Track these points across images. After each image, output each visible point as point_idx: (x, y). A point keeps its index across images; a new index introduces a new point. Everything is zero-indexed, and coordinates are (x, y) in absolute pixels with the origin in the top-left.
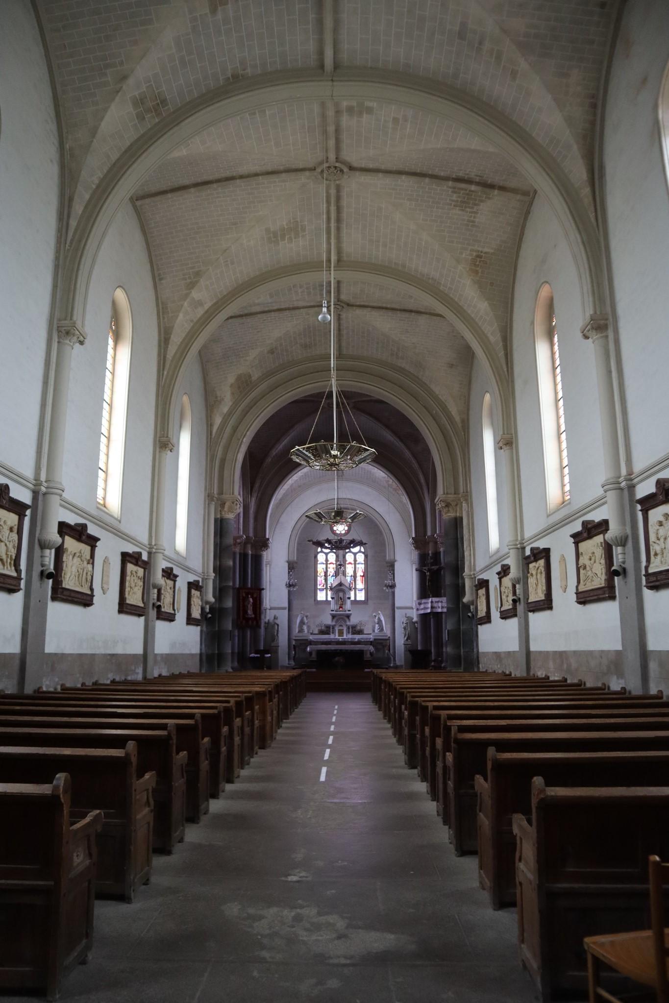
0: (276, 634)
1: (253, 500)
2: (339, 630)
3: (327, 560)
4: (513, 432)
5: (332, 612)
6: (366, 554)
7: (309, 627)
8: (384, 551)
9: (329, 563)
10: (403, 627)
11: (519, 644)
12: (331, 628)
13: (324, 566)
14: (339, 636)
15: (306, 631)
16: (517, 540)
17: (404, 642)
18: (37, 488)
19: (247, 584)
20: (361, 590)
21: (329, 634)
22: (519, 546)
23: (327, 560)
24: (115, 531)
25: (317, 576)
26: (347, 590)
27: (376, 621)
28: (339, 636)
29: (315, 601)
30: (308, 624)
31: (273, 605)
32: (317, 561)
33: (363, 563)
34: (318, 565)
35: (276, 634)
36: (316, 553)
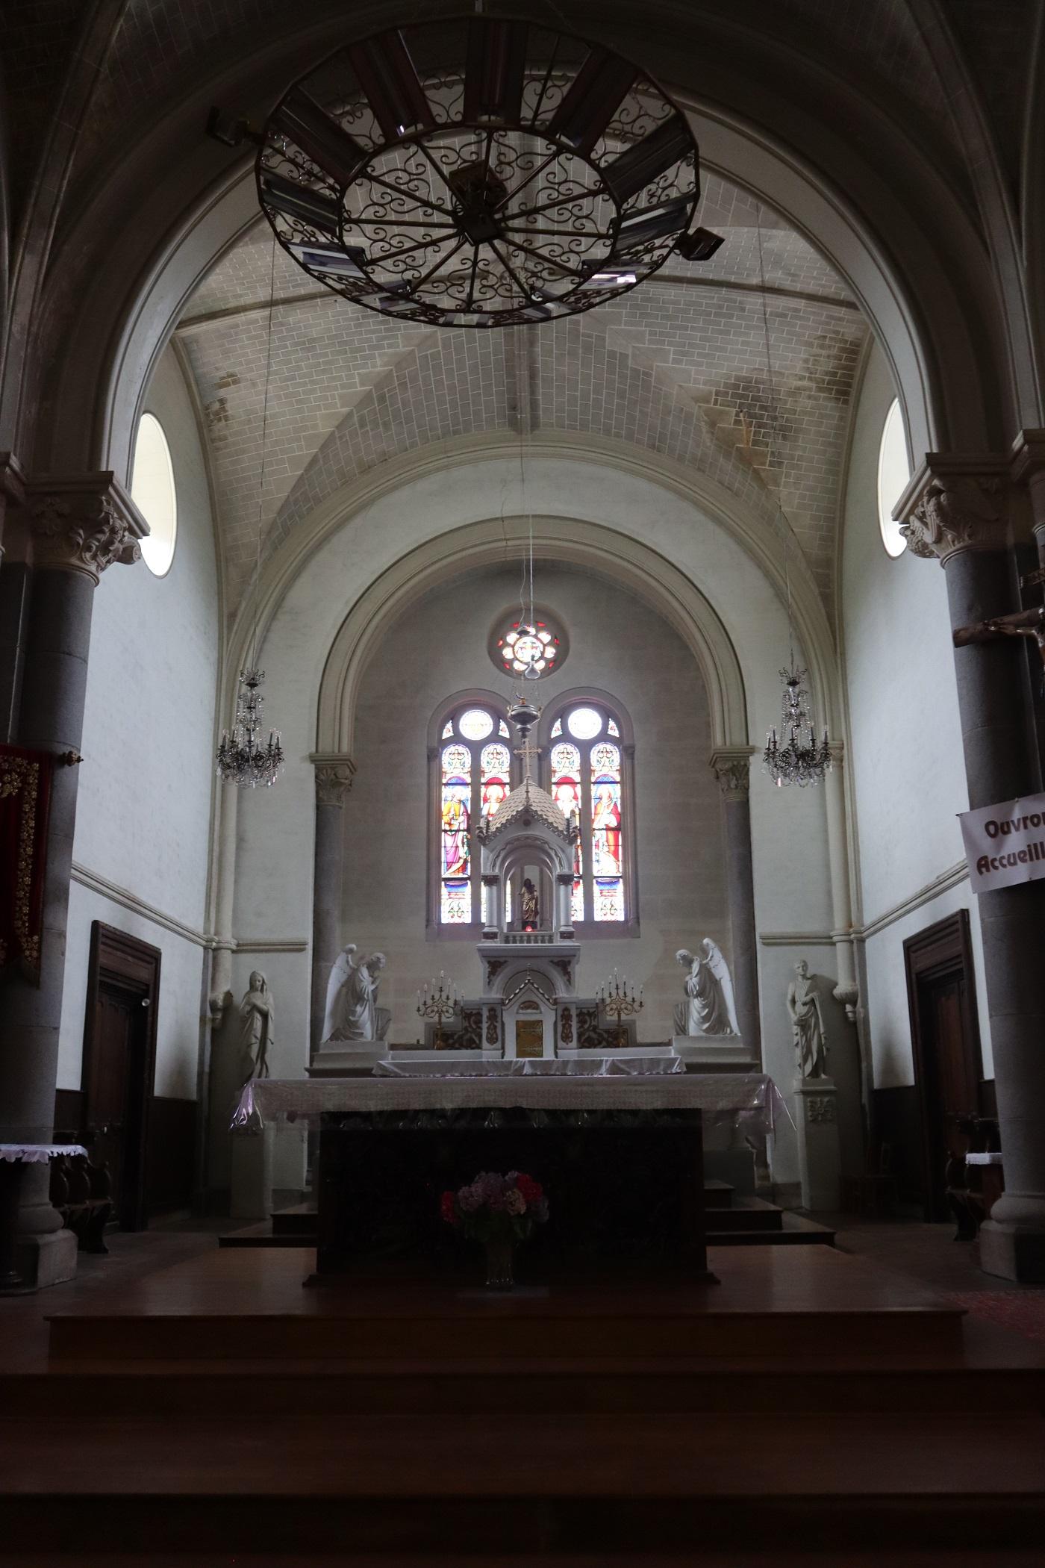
1: (30, 267)
3: (476, 771)
4: (845, 739)
6: (627, 742)
7: (382, 1017)
9: (483, 780)
10: (794, 1018)
12: (485, 1013)
13: (466, 793)
14: (520, 1053)
15: (368, 1031)
16: (850, 926)
17: (804, 1082)
18: (208, 943)
20: (612, 881)
21: (473, 1044)
22: (853, 936)
23: (476, 771)
24: (188, 934)
25: (440, 831)
27: (693, 981)
29: (428, 921)
30: (381, 1002)
31: (252, 935)
33: (618, 779)
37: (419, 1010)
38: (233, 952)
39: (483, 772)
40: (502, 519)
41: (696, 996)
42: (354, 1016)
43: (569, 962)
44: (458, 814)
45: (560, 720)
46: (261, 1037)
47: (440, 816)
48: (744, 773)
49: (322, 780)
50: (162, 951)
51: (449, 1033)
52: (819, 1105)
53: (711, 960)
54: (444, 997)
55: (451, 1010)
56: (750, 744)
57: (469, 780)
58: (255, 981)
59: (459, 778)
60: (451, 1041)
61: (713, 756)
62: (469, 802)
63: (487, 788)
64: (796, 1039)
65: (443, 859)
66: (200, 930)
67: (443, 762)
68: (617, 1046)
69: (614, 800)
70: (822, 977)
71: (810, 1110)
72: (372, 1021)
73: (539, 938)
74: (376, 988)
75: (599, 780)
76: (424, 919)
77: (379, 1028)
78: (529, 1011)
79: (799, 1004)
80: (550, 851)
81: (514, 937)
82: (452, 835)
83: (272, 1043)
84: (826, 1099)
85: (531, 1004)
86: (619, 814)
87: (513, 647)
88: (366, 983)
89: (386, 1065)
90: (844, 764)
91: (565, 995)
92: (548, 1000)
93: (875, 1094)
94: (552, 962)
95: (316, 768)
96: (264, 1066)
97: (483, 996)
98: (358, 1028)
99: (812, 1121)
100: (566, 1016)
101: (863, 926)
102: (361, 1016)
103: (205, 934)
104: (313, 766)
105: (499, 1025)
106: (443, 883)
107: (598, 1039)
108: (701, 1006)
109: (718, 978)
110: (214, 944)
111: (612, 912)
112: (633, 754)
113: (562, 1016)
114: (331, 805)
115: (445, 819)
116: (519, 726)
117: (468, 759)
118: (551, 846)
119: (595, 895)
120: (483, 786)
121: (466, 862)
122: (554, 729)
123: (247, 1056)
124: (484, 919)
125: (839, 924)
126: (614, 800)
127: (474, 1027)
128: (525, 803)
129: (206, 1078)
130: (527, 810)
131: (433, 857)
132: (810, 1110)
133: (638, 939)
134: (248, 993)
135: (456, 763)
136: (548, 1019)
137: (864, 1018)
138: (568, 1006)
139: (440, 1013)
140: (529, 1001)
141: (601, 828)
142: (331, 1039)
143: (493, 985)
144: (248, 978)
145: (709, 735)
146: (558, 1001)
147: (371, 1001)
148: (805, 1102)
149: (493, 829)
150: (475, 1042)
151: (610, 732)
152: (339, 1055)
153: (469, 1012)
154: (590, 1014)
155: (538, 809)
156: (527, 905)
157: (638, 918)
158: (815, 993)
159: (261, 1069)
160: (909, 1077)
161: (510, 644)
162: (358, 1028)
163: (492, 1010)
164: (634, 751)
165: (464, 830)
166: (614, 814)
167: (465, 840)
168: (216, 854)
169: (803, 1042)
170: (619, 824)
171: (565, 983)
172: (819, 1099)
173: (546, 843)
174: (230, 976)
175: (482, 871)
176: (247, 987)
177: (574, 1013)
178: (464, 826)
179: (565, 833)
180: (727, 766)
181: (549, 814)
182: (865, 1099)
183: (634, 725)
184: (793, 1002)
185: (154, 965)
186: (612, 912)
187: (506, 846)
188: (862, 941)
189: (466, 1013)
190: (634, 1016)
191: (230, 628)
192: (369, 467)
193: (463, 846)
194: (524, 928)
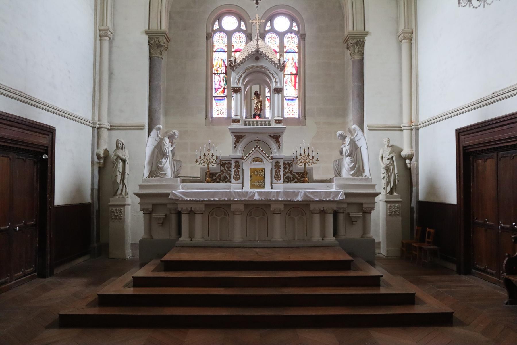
0: (119, 180)
2: (253, 172)
3: (230, 45)
5: (235, 125)
6: (301, 32)
7: (177, 164)
8: (342, 18)
10: (383, 166)
12: (233, 164)
13: (225, 56)
14: (252, 186)
16: (411, 122)
18: (94, 125)
19: (474, 269)
20: (293, 99)
21: (226, 180)
23: (230, 45)
26: (273, 69)
27: (346, 148)
28: (252, 186)
29: (206, 116)
31: (119, 121)
32: (213, 46)
35: (119, 180)
36: (210, 31)
37: (197, 161)
38: (108, 129)
41: (347, 156)
42: (161, 164)
43: (280, 136)
44: (221, 65)
45: (270, 22)
48: (362, 45)
49: (152, 44)
50: (56, 128)
51: (214, 173)
52: (393, 208)
53: (356, 137)
55: (214, 162)
56: (366, 30)
57: (226, 50)
58: (119, 144)
59: (221, 48)
63: (235, 54)
64: (382, 176)
65: (214, 87)
66: (89, 117)
67: (214, 41)
68: (304, 182)
69: (295, 61)
70: (396, 146)
71: (389, 210)
72: (171, 168)
73: (263, 123)
74: (174, 149)
75: (288, 51)
76: (205, 115)
77: (175, 171)
78: (257, 163)
79: (385, 159)
80: (270, 74)
81: (249, 122)
82: (218, 76)
83: (128, 175)
84: (397, 205)
85: (258, 159)
86: (297, 67)
88: (168, 147)
89: (176, 193)
90: (412, 41)
91: (277, 154)
92: (268, 157)
93: (421, 204)
94: (270, 136)
95: (148, 37)
96: (124, 186)
97: (231, 154)
98: (163, 171)
99: (389, 215)
100: (277, 166)
101: (419, 122)
102: (164, 165)
103: (92, 120)
104: (147, 36)
105: (240, 170)
106: (214, 98)
107: (293, 177)
108: (350, 161)
109: (359, 146)
110: (97, 126)
111: (293, 113)
112: (304, 38)
113: (275, 166)
114: (156, 57)
115: (215, 68)
117: (226, 40)
118: (270, 72)
119: (285, 105)
121: (224, 88)
122: (267, 26)
123: (115, 181)
125: (405, 121)
126: (295, 61)
127: (227, 170)
128: (256, 47)
129: (96, 192)
130: (257, 51)
132: (389, 210)
133: (305, 126)
134: (115, 150)
135: (220, 41)
136: (268, 167)
138: (279, 160)
139: (208, 163)
140: (258, 158)
141: (288, 74)
142: (149, 177)
143: (238, 148)
144: (116, 143)
145: (342, 27)
146: (274, 157)
148: (386, 206)
149: (238, 62)
150: (227, 178)
151: (294, 28)
152: (154, 185)
153: (224, 162)
154: (289, 164)
156: (256, 105)
157: (305, 116)
158: (393, 154)
160: (452, 198)
163: (237, 162)
165: (224, 74)
166: (294, 67)
167: (224, 78)
170: (297, 72)
171: (277, 148)
174: (107, 142)
175: (232, 85)
176: (115, 147)
177: (281, 164)
178: (224, 71)
180: (354, 41)
181: (269, 55)
182: (414, 204)
183: (306, 25)
184: (382, 158)
185: (50, 136)
186: (293, 113)
187: (245, 71)
188: (418, 129)
189: (222, 163)
190: (313, 166)
193: (223, 81)
194: (254, 117)
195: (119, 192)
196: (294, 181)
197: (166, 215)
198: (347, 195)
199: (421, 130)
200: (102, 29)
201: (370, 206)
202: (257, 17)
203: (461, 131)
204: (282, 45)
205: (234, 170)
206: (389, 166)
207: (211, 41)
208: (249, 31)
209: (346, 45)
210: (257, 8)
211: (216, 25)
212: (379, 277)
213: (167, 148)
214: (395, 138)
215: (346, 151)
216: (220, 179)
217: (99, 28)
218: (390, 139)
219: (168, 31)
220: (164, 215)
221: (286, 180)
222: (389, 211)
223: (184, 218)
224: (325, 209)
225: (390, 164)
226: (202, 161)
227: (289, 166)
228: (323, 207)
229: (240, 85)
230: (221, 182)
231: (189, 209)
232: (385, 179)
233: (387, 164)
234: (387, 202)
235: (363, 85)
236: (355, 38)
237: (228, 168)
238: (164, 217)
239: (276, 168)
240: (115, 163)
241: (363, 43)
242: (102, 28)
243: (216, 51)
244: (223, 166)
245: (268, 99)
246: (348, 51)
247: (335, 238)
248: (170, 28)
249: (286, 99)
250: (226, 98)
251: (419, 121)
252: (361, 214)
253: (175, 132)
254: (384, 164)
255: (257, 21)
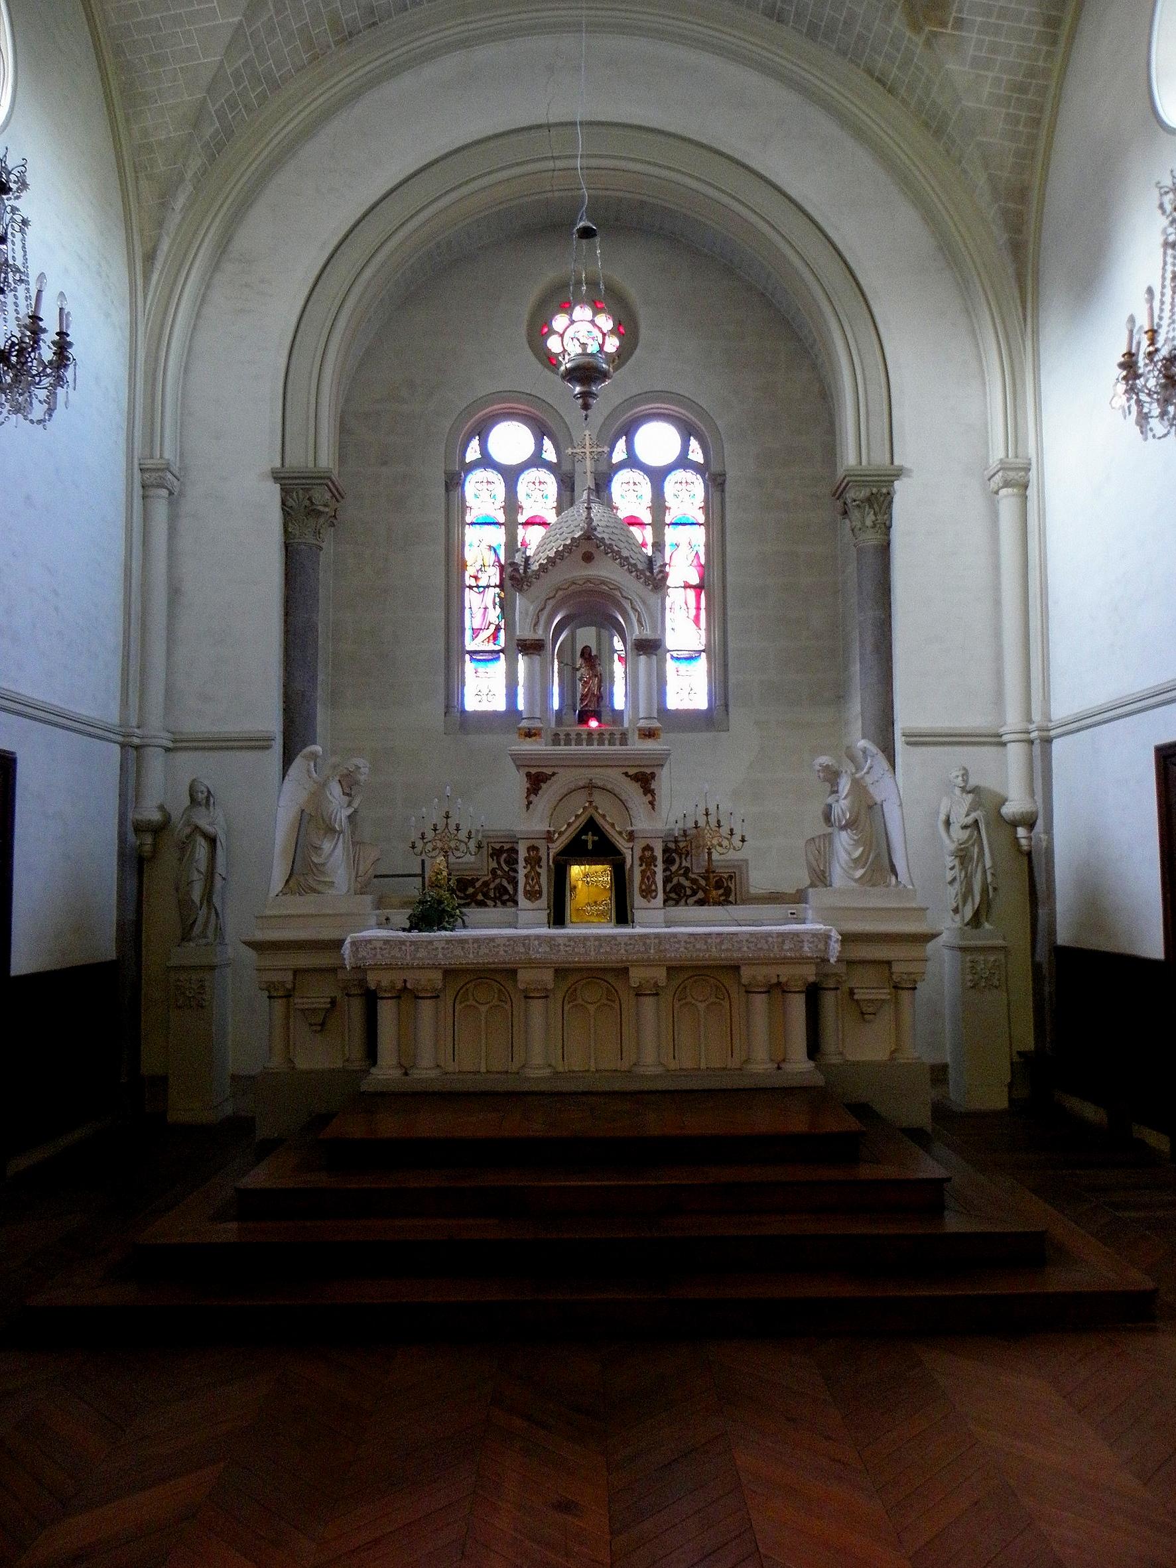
3: (512, 505)
6: (715, 468)
8: (831, 429)
9: (522, 518)
11: (14, 806)
13: (498, 536)
16: (1030, 721)
23: (512, 505)
25: (462, 587)
26: (631, 586)
27: (842, 806)
31: (192, 726)
32: (464, 508)
33: (702, 519)
34: (469, 530)
39: (521, 507)
40: (549, 126)
43: (653, 775)
46: (207, 871)
47: (463, 566)
48: (886, 504)
53: (868, 773)
54: (452, 827)
56: (896, 462)
58: (197, 792)
60: (471, 890)
61: (844, 479)
62: (503, 548)
64: (949, 875)
65: (467, 625)
74: (355, 811)
79: (955, 829)
80: (624, 602)
82: (480, 593)
83: (224, 879)
87: (562, 336)
90: (1028, 492)
94: (626, 774)
101: (1050, 721)
102: (330, 855)
106: (467, 657)
107: (691, 888)
113: (641, 859)
115: (470, 571)
116: (578, 389)
120: (520, 527)
121: (498, 629)
124: (521, 706)
125: (1013, 720)
127: (507, 869)
131: (454, 624)
135: (485, 495)
137: (1047, 849)
142: (283, 892)
145: (831, 450)
147: (348, 832)
149: (535, 567)
150: (506, 891)
151: (691, 456)
153: (497, 846)
155: (606, 536)
157: (726, 706)
158: (978, 812)
159: (209, 913)
161: (557, 333)
162: (323, 873)
164: (724, 481)
165: (496, 586)
167: (497, 600)
168: (136, 607)
169: (962, 878)
170: (702, 578)
172: (982, 958)
173: (619, 589)
176: (187, 802)
177: (659, 853)
178: (496, 580)
179: (648, 574)
180: (864, 493)
181: (622, 545)
182: (1042, 955)
184: (948, 823)
188: (1048, 741)
189: (493, 849)
191: (147, 277)
192: (351, 34)
193: (494, 608)
195: (197, 930)
196: (695, 898)
197: (333, 1002)
198: (848, 938)
199: (1057, 745)
200: (148, 466)
201: (911, 968)
202: (587, 438)
203: (1170, 752)
204: (659, 506)
205: (525, 871)
206: (967, 848)
207: (458, 493)
208: (566, 467)
209: (839, 503)
210: (586, 419)
211: (474, 450)
212: (938, 1184)
213: (335, 812)
214: (980, 762)
215: (840, 812)
216: (486, 895)
217: (140, 464)
218: (970, 772)
219: (336, 472)
220: (329, 1000)
221: (673, 895)
222: (970, 977)
223: (386, 1012)
224: (783, 979)
225: (970, 842)
226: (429, 847)
227: (681, 858)
228: (778, 976)
229: (540, 634)
230: (489, 902)
231: (399, 985)
232: (957, 885)
233: (960, 842)
234: (963, 949)
235: (890, 616)
236: (866, 486)
237: (507, 862)
238: (329, 1006)
239: (644, 864)
240: (185, 846)
241: (889, 498)
242: (149, 463)
243: (472, 524)
244: (495, 858)
245: (620, 658)
246: (847, 521)
247: (812, 1064)
248: (342, 459)
249: (672, 657)
250: (501, 654)
251: (1054, 717)
252: (884, 994)
253: (359, 765)
254: (953, 842)
255: (587, 450)
